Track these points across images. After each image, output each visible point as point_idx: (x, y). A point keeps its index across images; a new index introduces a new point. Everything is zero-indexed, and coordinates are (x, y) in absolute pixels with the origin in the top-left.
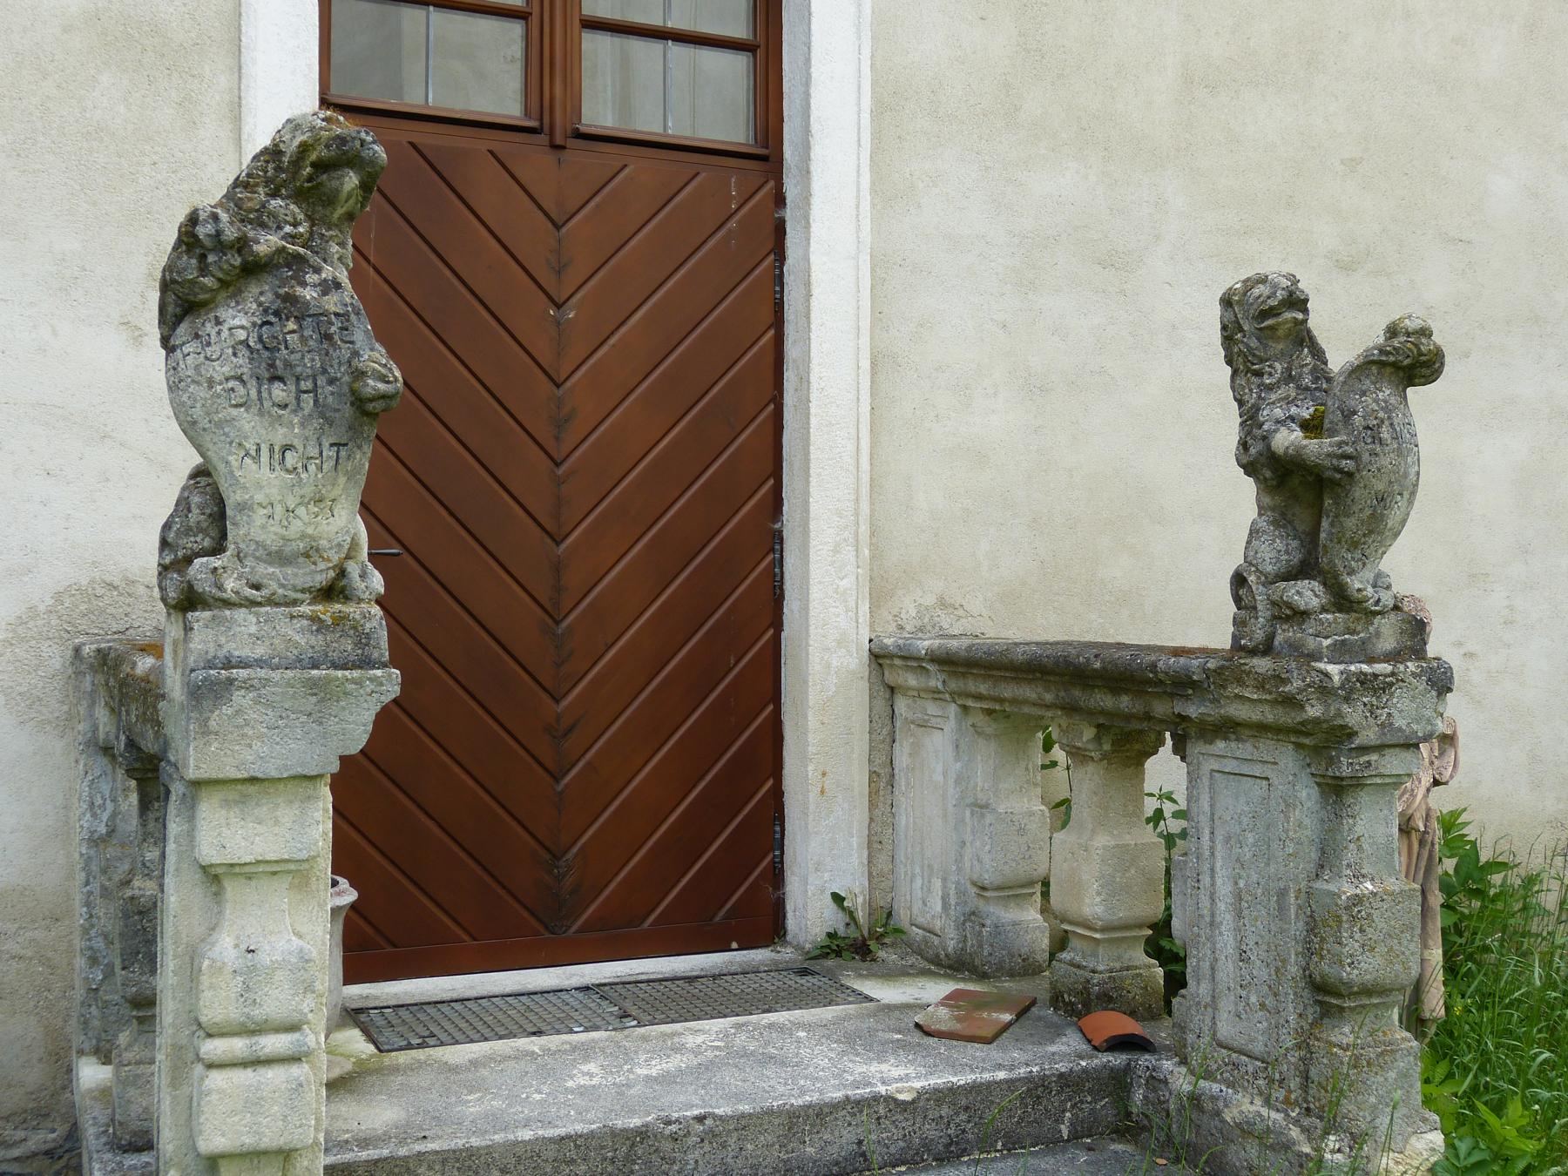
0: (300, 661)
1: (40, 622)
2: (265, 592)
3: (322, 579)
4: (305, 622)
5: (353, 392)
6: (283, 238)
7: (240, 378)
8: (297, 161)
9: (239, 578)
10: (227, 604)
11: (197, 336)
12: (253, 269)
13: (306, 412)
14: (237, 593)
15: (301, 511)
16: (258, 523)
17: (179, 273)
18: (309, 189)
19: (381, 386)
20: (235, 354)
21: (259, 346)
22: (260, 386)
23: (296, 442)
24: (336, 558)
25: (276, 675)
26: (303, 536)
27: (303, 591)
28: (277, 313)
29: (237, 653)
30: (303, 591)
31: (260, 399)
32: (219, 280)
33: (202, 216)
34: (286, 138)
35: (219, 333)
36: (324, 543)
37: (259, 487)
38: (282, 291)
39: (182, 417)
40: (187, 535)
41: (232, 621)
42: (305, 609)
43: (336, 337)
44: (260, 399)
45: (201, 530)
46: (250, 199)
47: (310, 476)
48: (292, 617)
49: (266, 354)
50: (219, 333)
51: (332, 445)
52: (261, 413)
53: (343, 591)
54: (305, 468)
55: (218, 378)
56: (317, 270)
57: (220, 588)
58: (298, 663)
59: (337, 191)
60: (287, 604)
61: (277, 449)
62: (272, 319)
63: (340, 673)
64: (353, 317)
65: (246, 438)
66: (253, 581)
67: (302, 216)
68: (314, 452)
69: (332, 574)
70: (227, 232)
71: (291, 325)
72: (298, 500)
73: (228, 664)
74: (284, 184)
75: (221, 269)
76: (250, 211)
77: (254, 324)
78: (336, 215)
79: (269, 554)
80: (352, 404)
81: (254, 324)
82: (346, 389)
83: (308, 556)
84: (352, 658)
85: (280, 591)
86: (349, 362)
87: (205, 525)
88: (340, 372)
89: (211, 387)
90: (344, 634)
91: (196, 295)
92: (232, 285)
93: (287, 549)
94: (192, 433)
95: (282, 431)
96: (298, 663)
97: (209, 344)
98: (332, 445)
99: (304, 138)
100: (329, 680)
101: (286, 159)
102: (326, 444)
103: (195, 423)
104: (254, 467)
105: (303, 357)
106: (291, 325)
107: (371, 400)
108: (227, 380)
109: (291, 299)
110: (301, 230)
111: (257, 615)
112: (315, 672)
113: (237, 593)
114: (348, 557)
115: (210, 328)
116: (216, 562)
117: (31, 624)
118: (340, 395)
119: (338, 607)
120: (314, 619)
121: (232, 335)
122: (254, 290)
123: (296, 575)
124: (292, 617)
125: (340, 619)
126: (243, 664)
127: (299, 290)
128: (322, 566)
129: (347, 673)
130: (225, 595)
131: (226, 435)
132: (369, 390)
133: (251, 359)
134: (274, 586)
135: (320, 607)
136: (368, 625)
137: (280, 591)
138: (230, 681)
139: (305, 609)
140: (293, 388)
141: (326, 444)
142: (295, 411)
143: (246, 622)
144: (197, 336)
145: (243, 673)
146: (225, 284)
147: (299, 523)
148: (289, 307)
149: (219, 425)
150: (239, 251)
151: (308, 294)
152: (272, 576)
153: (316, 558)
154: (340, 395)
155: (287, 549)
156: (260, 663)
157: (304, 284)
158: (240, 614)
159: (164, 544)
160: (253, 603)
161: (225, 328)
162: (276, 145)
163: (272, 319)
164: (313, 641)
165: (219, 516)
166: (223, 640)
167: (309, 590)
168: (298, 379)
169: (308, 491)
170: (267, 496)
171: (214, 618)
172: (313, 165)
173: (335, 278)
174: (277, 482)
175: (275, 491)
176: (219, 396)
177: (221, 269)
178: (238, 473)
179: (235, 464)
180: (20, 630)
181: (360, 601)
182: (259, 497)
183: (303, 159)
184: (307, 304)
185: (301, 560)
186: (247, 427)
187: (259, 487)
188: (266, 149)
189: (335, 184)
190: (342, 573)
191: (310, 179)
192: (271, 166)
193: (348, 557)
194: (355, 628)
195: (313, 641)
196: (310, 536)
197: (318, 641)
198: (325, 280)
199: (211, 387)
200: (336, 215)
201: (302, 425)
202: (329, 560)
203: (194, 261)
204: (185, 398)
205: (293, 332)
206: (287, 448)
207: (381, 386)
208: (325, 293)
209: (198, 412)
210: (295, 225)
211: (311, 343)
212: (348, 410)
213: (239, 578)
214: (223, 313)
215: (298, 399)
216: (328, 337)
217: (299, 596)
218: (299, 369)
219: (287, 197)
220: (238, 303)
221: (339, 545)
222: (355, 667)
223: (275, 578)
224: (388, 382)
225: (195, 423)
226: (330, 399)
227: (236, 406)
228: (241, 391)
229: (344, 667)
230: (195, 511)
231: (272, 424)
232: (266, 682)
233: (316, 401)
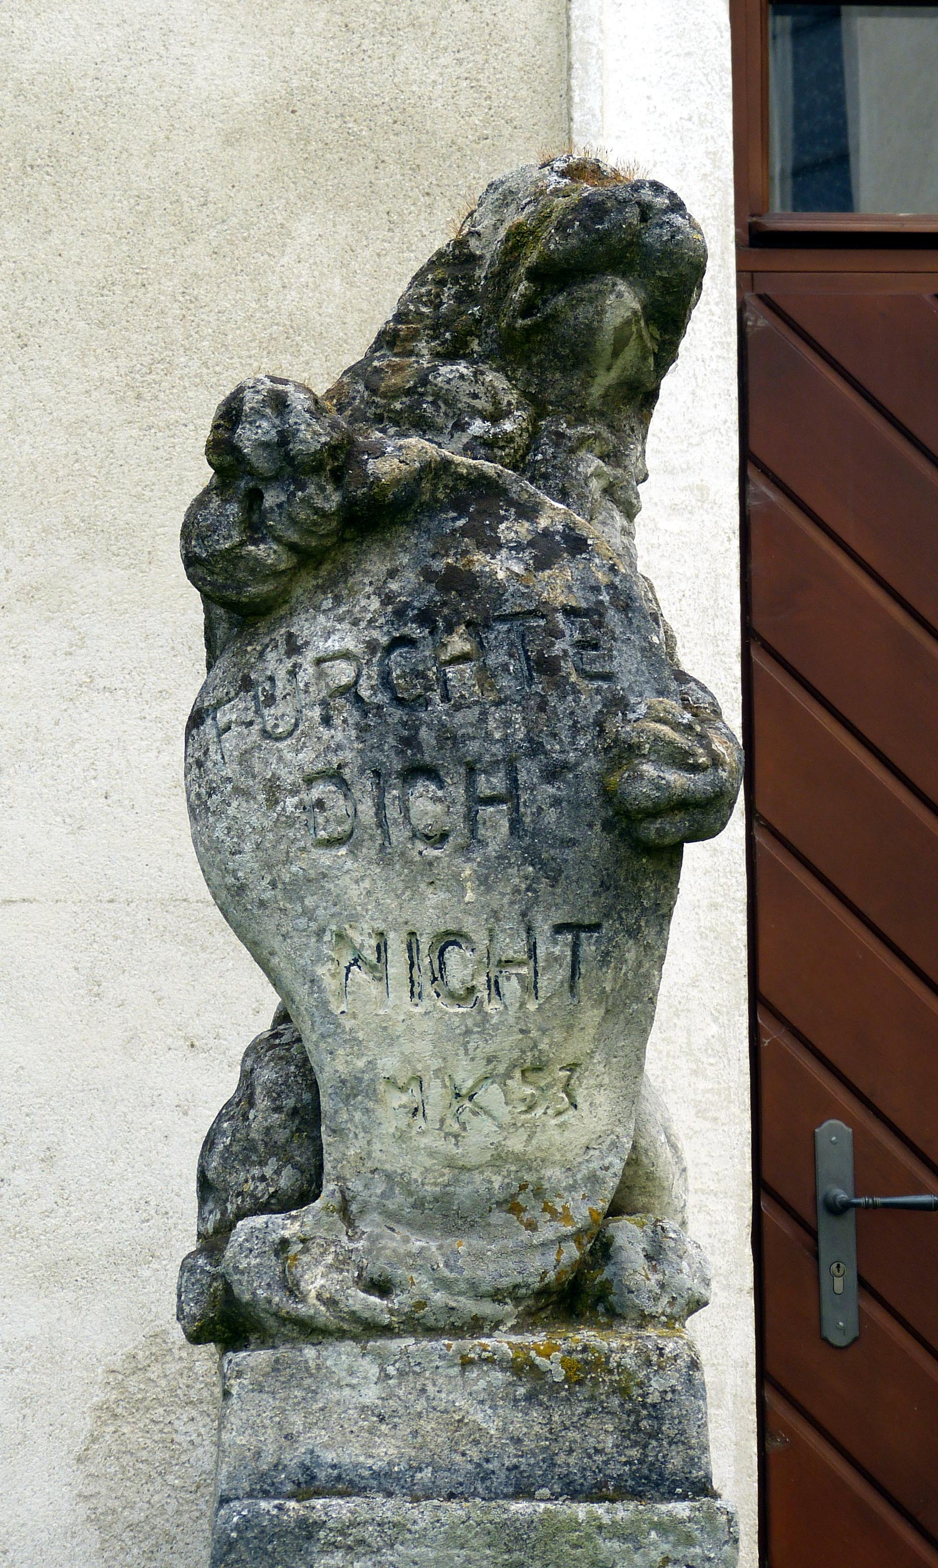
0: (486, 1476)
1: (173, 1368)
2: (399, 1300)
3: (544, 1256)
4: (499, 1377)
5: (608, 796)
6: (467, 449)
7: (335, 776)
8: (501, 277)
9: (339, 1266)
10: (310, 1331)
11: (247, 684)
12: (373, 516)
13: (492, 849)
14: (331, 1303)
15: (491, 1095)
16: (389, 1128)
17: (202, 538)
18: (528, 332)
19: (676, 779)
20: (326, 720)
21: (382, 698)
22: (382, 791)
23: (469, 925)
24: (582, 1209)
25: (421, 1515)
26: (499, 1159)
27: (497, 1296)
28: (425, 618)
29: (329, 1456)
30: (497, 1296)
31: (382, 823)
32: (292, 547)
33: (251, 401)
34: (485, 223)
35: (293, 673)
36: (553, 1174)
37: (388, 1038)
38: (439, 565)
39: (215, 873)
40: (246, 1162)
41: (319, 1373)
42: (501, 1342)
43: (567, 666)
44: (382, 823)
45: (274, 1149)
46: (397, 369)
47: (509, 1003)
48: (466, 1363)
49: (397, 715)
50: (293, 673)
51: (559, 929)
52: (385, 857)
53: (602, 1294)
54: (495, 987)
55: (288, 778)
56: (528, 512)
57: (292, 1289)
58: (480, 1483)
59: (592, 330)
60: (456, 1331)
61: (425, 943)
62: (414, 630)
63: (581, 1510)
64: (613, 617)
65: (353, 919)
66: (374, 1270)
67: (513, 397)
68: (515, 948)
69: (572, 1252)
70: (305, 434)
71: (458, 644)
72: (481, 1068)
73: (308, 1485)
74: (477, 327)
75: (293, 521)
76: (394, 394)
77: (372, 646)
78: (596, 391)
79: (419, 1205)
80: (608, 826)
81: (372, 646)
82: (590, 790)
83: (513, 1206)
84: (614, 1470)
85: (439, 1298)
86: (599, 724)
87: (281, 1136)
88: (579, 752)
89: (272, 801)
90: (596, 1408)
91: (240, 586)
92: (323, 558)
93: (463, 1192)
94: (238, 915)
95: (435, 897)
96: (480, 1483)
97: (270, 700)
98: (559, 929)
99: (521, 218)
100: (554, 1529)
101: (480, 273)
102: (543, 928)
103: (242, 889)
104: (374, 989)
105: (484, 715)
106: (458, 644)
107: (654, 813)
108: (310, 781)
109: (460, 582)
110: (508, 426)
111: (381, 1358)
112: (519, 1507)
113: (331, 1303)
114: (616, 1210)
115: (275, 664)
116: (287, 1226)
117: (155, 1372)
118: (576, 805)
119: (587, 1335)
120: (521, 1367)
121: (321, 675)
122: (377, 566)
123: (479, 1256)
124: (466, 1363)
125: (585, 1369)
126: (346, 1485)
127: (480, 560)
128: (547, 1232)
129: (600, 1509)
130: (302, 1310)
131: (309, 914)
132: (645, 788)
133: (363, 729)
134: (423, 1283)
135: (539, 1338)
136: (656, 1384)
137: (439, 1298)
138: (308, 1529)
139: (501, 1342)
140: (459, 793)
141: (543, 928)
142: (464, 850)
143: (353, 1375)
144: (247, 684)
145: (338, 1509)
146: (306, 558)
147: (488, 1125)
148: (458, 599)
149: (294, 890)
150: (337, 477)
151: (502, 567)
152: (418, 1260)
153: (534, 1212)
154: (576, 805)
155: (463, 1192)
156: (385, 1482)
157: (492, 545)
158: (341, 1356)
159: (205, 1186)
160: (369, 1329)
161: (307, 659)
162: (460, 244)
163: (414, 630)
164: (518, 1423)
165: (307, 1118)
166: (297, 1421)
167: (512, 1293)
168: (471, 771)
169: (505, 1044)
170: (407, 1060)
171: (276, 1367)
172: (533, 274)
173: (570, 528)
174: (427, 1025)
175: (424, 1047)
176: (291, 822)
177: (293, 521)
178: (336, 1007)
179: (330, 984)
180: (133, 1383)
181: (645, 1319)
182: (389, 1064)
183: (514, 264)
184: (498, 591)
185: (498, 1217)
186: (355, 893)
187: (388, 1038)
188: (440, 254)
189: (583, 313)
190: (601, 1249)
191: (528, 309)
192: (448, 293)
193: (616, 1210)
194: (622, 1391)
195: (518, 1426)
196: (518, 1158)
197: (530, 1424)
198: (546, 534)
199: (272, 801)
200: (596, 391)
201: (484, 882)
202: (566, 1217)
203: (233, 509)
204: (219, 833)
205: (463, 658)
206: (450, 939)
207: (676, 779)
208: (542, 563)
209: (247, 863)
210: (495, 417)
211: (504, 682)
212: (596, 843)
213: (339, 1266)
214: (305, 626)
215: (471, 819)
216: (546, 666)
217: (488, 1308)
218: (473, 747)
219: (485, 357)
220: (338, 600)
221: (593, 1179)
222: (622, 1493)
223: (424, 1261)
224: (695, 768)
225: (242, 889)
226: (551, 815)
227: (330, 843)
228: (339, 805)
229: (595, 1494)
230: (262, 1103)
231: (410, 884)
232: (395, 1531)
233: (515, 824)
